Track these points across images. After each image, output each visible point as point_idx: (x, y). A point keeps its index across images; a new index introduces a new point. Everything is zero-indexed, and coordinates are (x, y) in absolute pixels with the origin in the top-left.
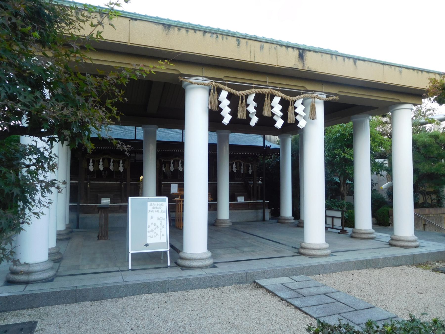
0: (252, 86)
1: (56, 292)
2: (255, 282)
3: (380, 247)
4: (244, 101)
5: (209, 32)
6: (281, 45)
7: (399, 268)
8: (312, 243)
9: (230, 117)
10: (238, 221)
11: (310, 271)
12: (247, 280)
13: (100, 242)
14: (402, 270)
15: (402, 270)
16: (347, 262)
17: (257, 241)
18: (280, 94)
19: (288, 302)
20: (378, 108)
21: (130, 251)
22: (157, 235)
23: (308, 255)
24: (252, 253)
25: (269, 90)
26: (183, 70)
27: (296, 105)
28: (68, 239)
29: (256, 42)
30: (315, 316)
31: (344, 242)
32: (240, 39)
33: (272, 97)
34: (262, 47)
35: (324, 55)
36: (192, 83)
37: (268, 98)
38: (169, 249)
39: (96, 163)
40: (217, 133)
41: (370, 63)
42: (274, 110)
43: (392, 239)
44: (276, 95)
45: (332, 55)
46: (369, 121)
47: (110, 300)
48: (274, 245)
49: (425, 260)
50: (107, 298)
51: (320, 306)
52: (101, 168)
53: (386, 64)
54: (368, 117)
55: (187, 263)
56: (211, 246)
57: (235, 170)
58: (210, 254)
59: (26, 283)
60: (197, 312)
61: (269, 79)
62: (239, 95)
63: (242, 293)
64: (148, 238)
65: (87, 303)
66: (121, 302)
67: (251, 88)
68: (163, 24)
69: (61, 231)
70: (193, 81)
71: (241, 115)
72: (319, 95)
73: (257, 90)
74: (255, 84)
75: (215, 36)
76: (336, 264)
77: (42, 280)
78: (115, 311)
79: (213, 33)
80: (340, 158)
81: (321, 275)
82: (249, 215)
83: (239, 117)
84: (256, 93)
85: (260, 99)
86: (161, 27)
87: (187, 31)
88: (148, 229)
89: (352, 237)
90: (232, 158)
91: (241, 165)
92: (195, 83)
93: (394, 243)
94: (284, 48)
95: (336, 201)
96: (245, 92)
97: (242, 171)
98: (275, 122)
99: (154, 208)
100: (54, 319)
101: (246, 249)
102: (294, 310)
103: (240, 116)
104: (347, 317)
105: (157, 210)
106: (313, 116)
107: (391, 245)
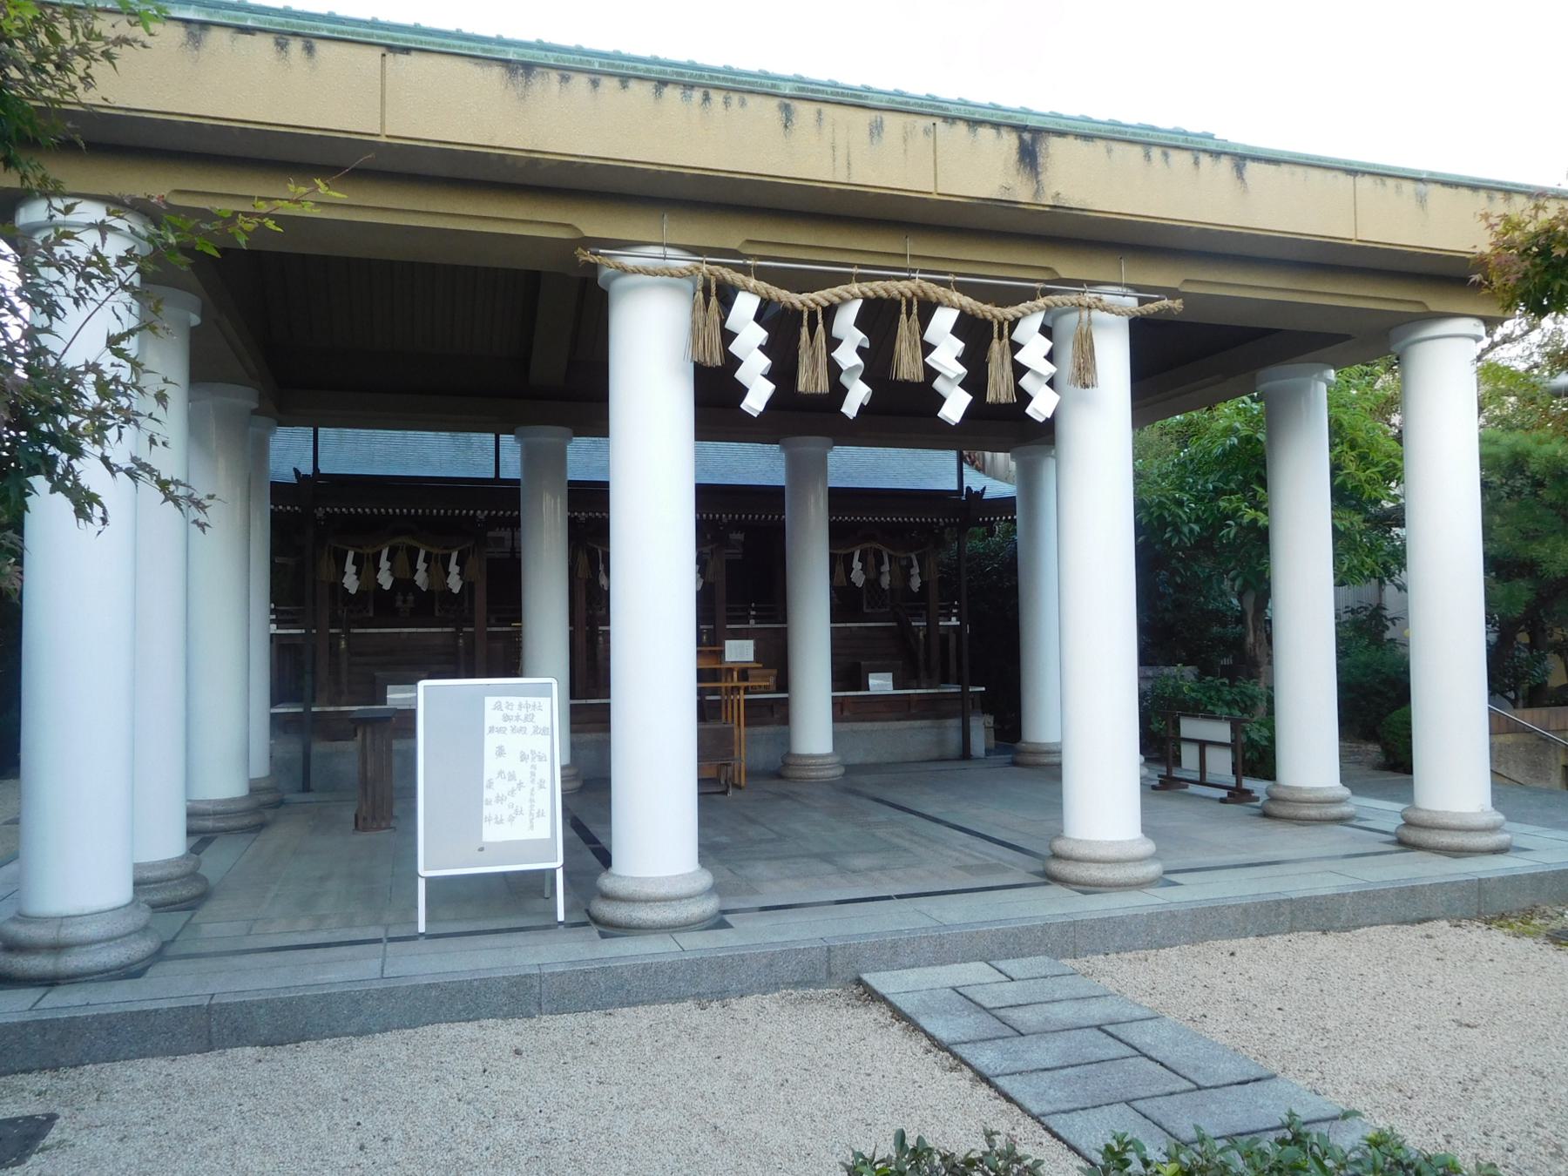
0: (851, 274)
1: (138, 1013)
2: (859, 982)
3: (1361, 851)
4: (820, 326)
5: (676, 83)
6: (950, 119)
7: (1419, 929)
8: (1086, 837)
9: (768, 388)
10: (871, 759)
11: (1071, 941)
12: (830, 974)
13: (363, 837)
14: (1428, 937)
15: (1428, 937)
16: (1216, 908)
17: (912, 833)
18: (956, 297)
19: (955, 1056)
20: (1347, 337)
21: (421, 871)
22: (519, 812)
23: (1077, 883)
24: (876, 874)
25: (912, 285)
26: (593, 224)
27: (1018, 335)
28: (259, 827)
29: (852, 110)
30: (1036, 1110)
31: (1235, 835)
32: (795, 104)
33: (927, 310)
34: (876, 130)
35: (1116, 146)
36: (625, 271)
37: (909, 314)
38: (560, 862)
39: (367, 566)
40: (784, 447)
41: (1299, 170)
42: (934, 359)
43: (1409, 824)
44: (939, 304)
45: (1147, 145)
46: (1323, 387)
47: (330, 1042)
48: (966, 846)
49: (1526, 903)
50: (319, 1037)
51: (1069, 1070)
52: (385, 580)
53: (1364, 173)
54: (1321, 371)
55: (619, 913)
56: (709, 851)
57: (858, 577)
58: (706, 879)
59: (50, 982)
60: (614, 1089)
61: (912, 246)
62: (799, 305)
63: (804, 1022)
64: (485, 825)
65: (249, 1050)
66: (361, 1049)
67: (845, 279)
68: (506, 63)
69: (233, 800)
70: (629, 262)
71: (811, 380)
72: (1104, 297)
73: (869, 288)
74: (957, 274)
75: (697, 95)
76: (1173, 915)
77: (108, 971)
78: (328, 1082)
79: (690, 86)
80: (1239, 525)
81: (1113, 956)
82: (914, 736)
83: (801, 388)
84: (866, 300)
85: (879, 319)
86: (497, 71)
87: (595, 84)
88: (488, 794)
89: (1266, 815)
90: (838, 534)
91: (880, 562)
92: (637, 271)
93: (1413, 835)
94: (962, 128)
95: (1223, 684)
96: (822, 296)
97: (885, 581)
98: (940, 400)
99: (507, 718)
100: (116, 1108)
101: (859, 862)
102: (968, 1084)
103: (804, 383)
104: (1156, 1115)
105: (519, 724)
106: (1085, 373)
107: (1404, 844)
